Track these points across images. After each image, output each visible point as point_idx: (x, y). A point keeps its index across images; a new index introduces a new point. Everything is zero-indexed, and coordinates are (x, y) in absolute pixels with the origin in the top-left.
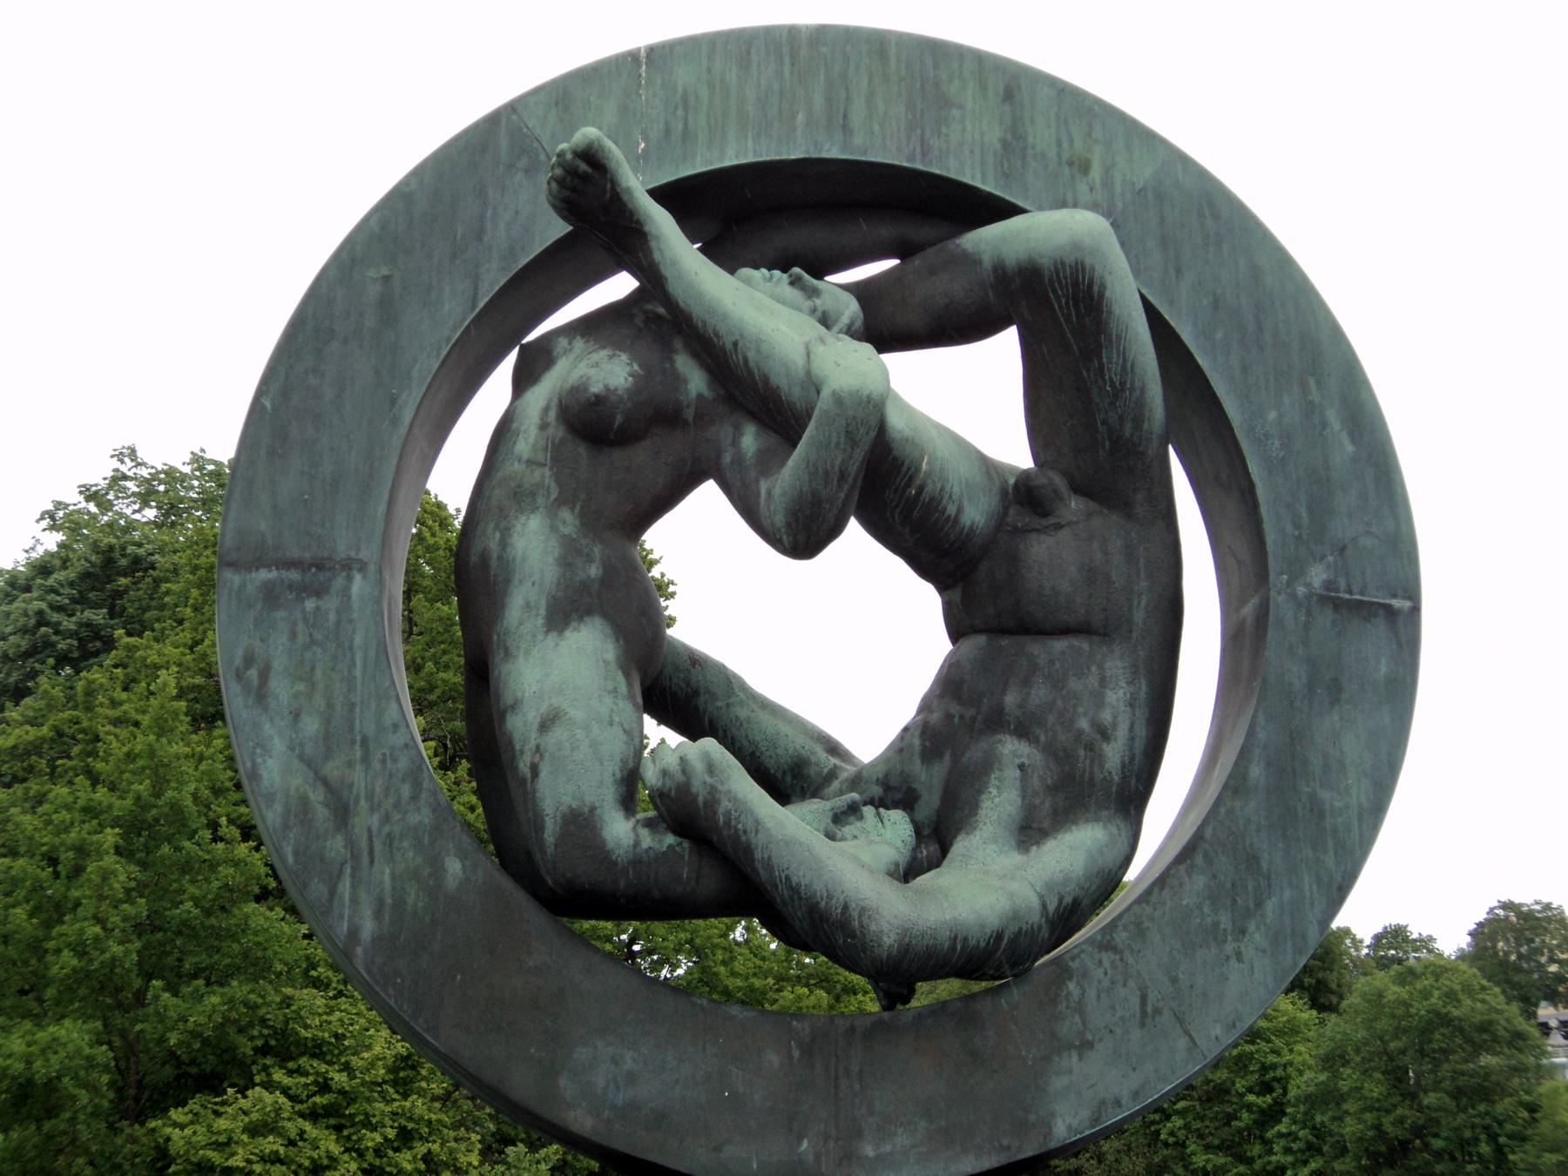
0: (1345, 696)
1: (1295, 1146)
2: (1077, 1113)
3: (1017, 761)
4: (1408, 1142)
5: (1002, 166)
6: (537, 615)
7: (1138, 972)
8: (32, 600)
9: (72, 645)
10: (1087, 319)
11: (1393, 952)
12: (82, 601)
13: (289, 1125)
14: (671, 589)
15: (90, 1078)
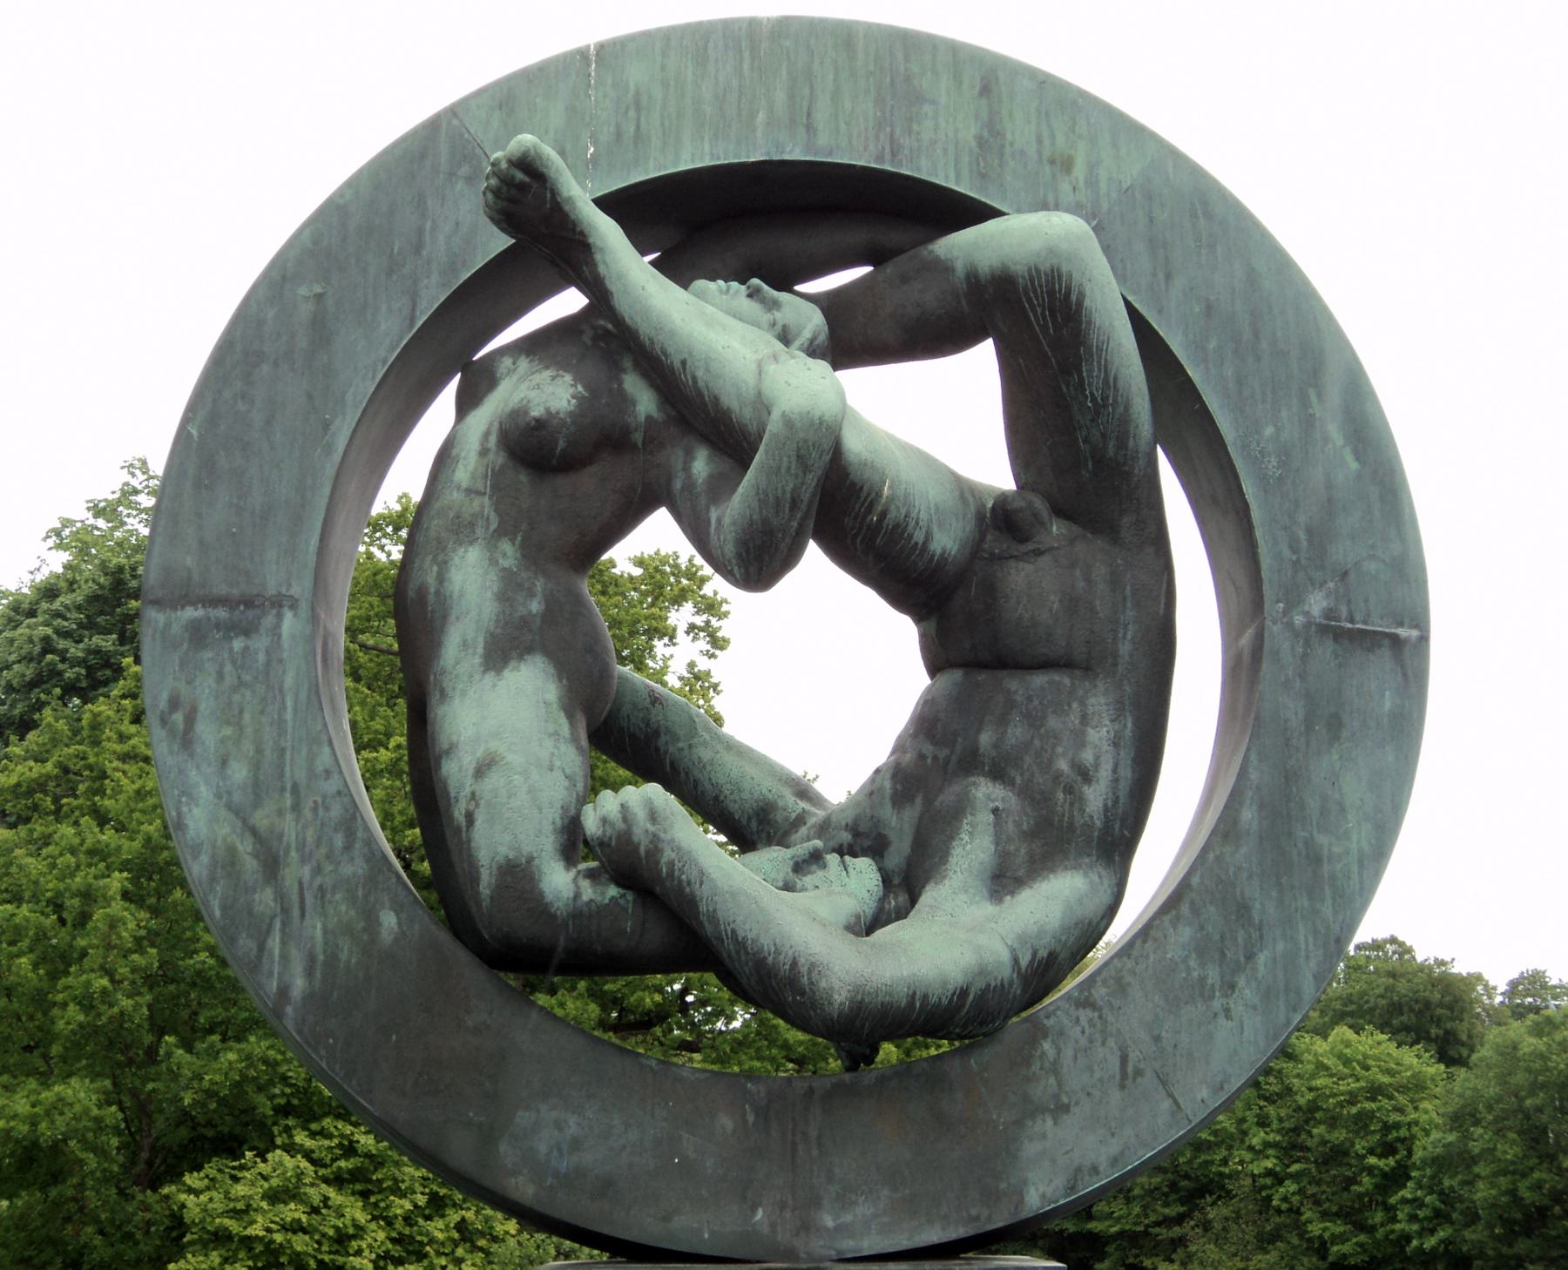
0: (1345, 733)
1: (1421, 1214)
2: (1051, 1181)
3: (992, 805)
4: (1547, 1208)
5: (978, 164)
6: (474, 654)
7: (1118, 1030)
8: (36, 625)
9: (79, 674)
10: (1065, 331)
11: (1530, 1000)
12: (90, 626)
13: (310, 1191)
14: (725, 608)
15: (98, 1141)
